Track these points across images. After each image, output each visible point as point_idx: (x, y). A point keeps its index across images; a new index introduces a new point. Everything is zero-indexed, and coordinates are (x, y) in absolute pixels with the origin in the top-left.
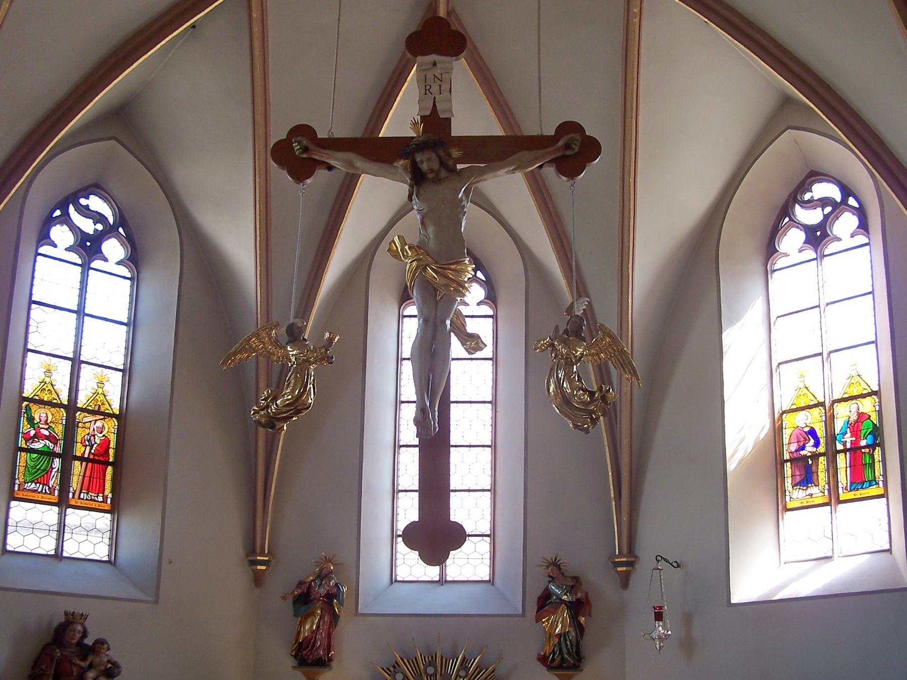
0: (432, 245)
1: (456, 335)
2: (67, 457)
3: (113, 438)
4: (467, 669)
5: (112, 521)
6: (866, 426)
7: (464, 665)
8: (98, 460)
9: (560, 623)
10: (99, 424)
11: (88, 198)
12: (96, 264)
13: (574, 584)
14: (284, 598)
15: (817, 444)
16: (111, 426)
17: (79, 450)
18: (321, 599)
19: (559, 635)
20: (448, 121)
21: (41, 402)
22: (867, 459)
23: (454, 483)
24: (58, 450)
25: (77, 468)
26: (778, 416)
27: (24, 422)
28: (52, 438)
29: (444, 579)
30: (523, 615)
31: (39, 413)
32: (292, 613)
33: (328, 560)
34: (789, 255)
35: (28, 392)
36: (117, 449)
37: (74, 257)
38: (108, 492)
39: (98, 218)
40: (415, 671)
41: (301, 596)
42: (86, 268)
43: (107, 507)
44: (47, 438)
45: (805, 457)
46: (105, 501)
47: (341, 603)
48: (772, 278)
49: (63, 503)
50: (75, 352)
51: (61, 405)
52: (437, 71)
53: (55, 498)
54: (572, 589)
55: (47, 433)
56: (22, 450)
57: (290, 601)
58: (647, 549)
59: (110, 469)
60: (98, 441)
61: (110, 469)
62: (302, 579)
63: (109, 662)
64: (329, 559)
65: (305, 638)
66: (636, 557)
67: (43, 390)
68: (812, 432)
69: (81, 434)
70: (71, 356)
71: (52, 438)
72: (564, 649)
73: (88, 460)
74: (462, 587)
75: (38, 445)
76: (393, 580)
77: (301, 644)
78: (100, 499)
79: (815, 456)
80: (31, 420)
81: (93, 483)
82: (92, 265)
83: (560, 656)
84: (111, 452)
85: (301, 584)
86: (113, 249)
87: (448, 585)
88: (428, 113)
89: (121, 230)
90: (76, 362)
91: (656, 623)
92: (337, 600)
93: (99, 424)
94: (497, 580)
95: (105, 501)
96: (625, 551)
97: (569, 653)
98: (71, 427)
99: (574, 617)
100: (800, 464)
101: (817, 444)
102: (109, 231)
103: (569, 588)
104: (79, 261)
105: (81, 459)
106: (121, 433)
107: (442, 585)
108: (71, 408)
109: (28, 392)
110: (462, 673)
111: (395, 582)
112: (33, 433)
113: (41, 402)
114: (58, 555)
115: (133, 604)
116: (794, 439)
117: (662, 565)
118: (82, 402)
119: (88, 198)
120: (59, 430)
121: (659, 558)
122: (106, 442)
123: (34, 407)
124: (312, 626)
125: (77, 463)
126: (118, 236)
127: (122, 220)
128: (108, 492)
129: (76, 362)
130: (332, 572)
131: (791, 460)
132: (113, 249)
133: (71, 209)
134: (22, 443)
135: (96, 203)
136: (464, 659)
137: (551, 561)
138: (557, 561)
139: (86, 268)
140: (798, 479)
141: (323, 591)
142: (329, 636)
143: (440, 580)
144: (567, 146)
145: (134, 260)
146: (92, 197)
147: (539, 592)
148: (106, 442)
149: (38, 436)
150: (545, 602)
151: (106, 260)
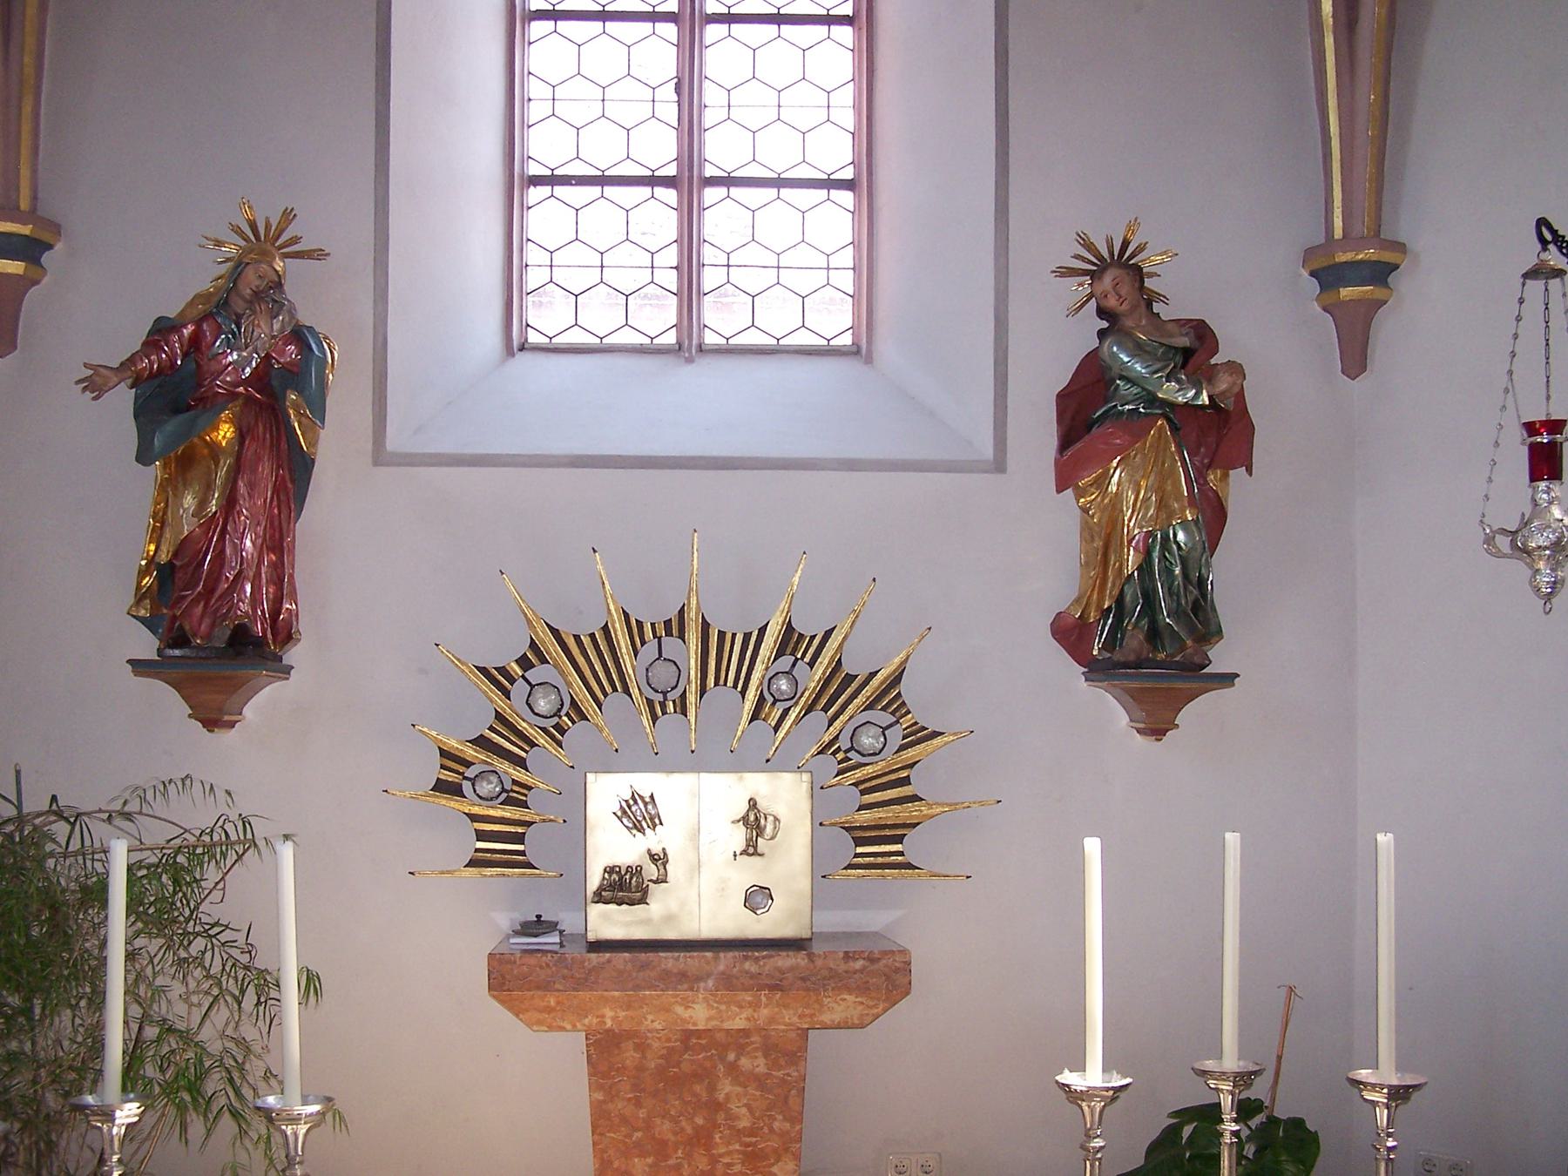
1: (596, 176)
18: (241, 389)
29: (695, 342)
32: (1237, 1057)
40: (605, 683)
47: (318, 408)
48: (217, 1013)
64: (268, 226)
74: (767, 370)
76: (515, 345)
83: (1144, 622)
87: (705, 365)
91: (1535, 490)
92: (300, 392)
94: (887, 348)
97: (1174, 613)
103: (1179, 359)
107: (690, 360)
111: (522, 348)
124: (203, 503)
137: (1106, 254)
138: (1116, 254)
143: (680, 344)
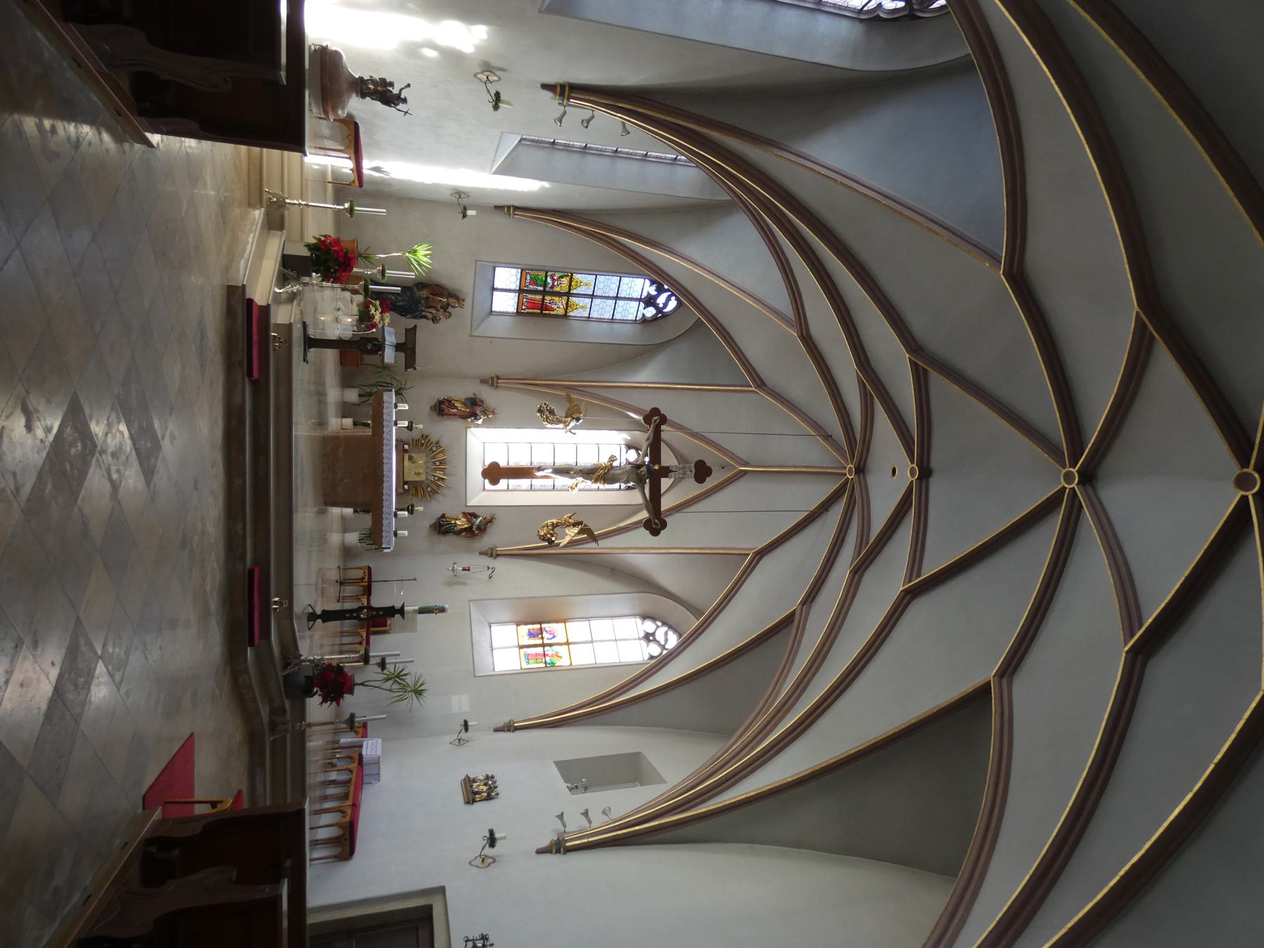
0: (612, 472)
2: (544, 293)
3: (555, 312)
4: (438, 480)
5: (513, 313)
6: (555, 660)
7: (440, 479)
8: (543, 306)
9: (462, 523)
10: (562, 307)
11: (659, 304)
12: (642, 305)
13: (483, 529)
14: (474, 394)
15: (548, 639)
16: (561, 311)
17: (548, 298)
19: (455, 523)
20: (667, 477)
21: (571, 281)
22: (539, 661)
23: (510, 480)
24: (547, 289)
25: (539, 297)
26: (157, 818)
27: (561, 274)
28: (553, 286)
30: (466, 506)
31: (565, 281)
33: (493, 412)
34: (561, 657)
35: (576, 277)
36: (549, 314)
37: (645, 294)
38: (527, 310)
39: (665, 305)
41: (475, 401)
42: (640, 300)
43: (519, 310)
44: (553, 284)
45: (542, 633)
46: (522, 309)
49: (521, 291)
50: (597, 296)
51: (570, 289)
52: (689, 473)
53: (523, 287)
54: (479, 528)
55: (555, 284)
56: (547, 273)
57: (473, 396)
58: (499, 564)
59: (539, 311)
60: (553, 306)
61: (539, 311)
62: (485, 402)
63: (440, 319)
65: (454, 404)
66: (495, 558)
67: (577, 282)
68: (554, 637)
69: (556, 299)
70: (595, 294)
71: (553, 286)
72: (448, 526)
73: (543, 302)
75: (549, 280)
77: (451, 401)
78: (523, 307)
79: (542, 638)
80: (562, 277)
81: (532, 305)
82: (641, 303)
84: (548, 312)
85: (482, 401)
86: (650, 312)
88: (671, 469)
89: (659, 315)
90: (592, 296)
93: (562, 307)
95: (522, 309)
96: (498, 553)
97: (447, 528)
98: (559, 294)
99: (465, 530)
100: (539, 632)
101: (548, 639)
102: (659, 310)
104: (643, 297)
105: (543, 299)
106: (557, 316)
108: (568, 294)
109: (576, 277)
110: (436, 478)
112: (555, 278)
113: (571, 281)
114: (494, 289)
115: (470, 320)
116: (551, 629)
117: (491, 570)
118: (573, 299)
119: (659, 304)
120: (557, 289)
121: (494, 569)
122: (553, 310)
123: (568, 278)
125: (541, 297)
126: (657, 314)
127: (665, 316)
128: (527, 310)
129: (592, 296)
130: (488, 416)
131: (541, 628)
132: (650, 312)
133: (669, 293)
134: (549, 274)
135: (673, 304)
136: (443, 479)
139: (640, 300)
140: (532, 631)
141: (478, 412)
142: (454, 415)
144: (655, 523)
145: (644, 320)
146: (676, 302)
147: (477, 513)
148: (553, 310)
149: (554, 280)
150: (471, 516)
151: (644, 309)
